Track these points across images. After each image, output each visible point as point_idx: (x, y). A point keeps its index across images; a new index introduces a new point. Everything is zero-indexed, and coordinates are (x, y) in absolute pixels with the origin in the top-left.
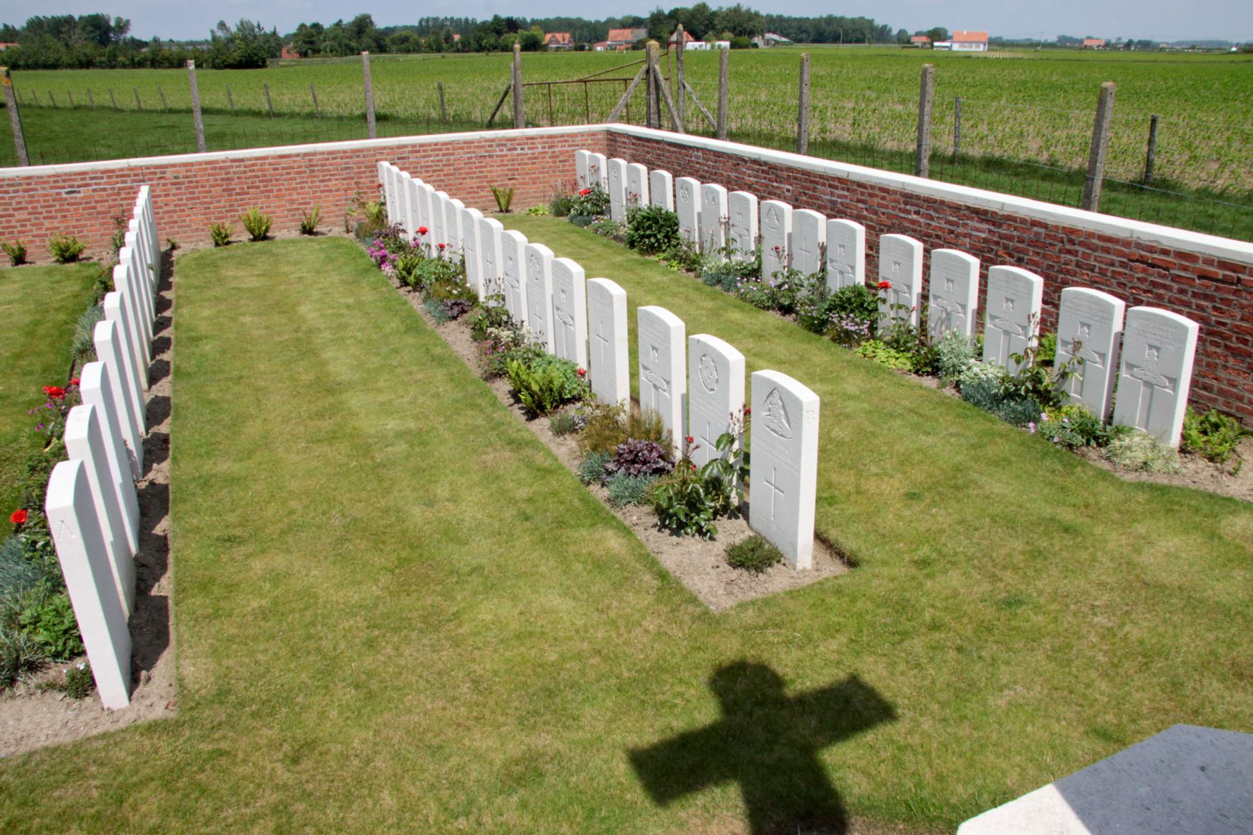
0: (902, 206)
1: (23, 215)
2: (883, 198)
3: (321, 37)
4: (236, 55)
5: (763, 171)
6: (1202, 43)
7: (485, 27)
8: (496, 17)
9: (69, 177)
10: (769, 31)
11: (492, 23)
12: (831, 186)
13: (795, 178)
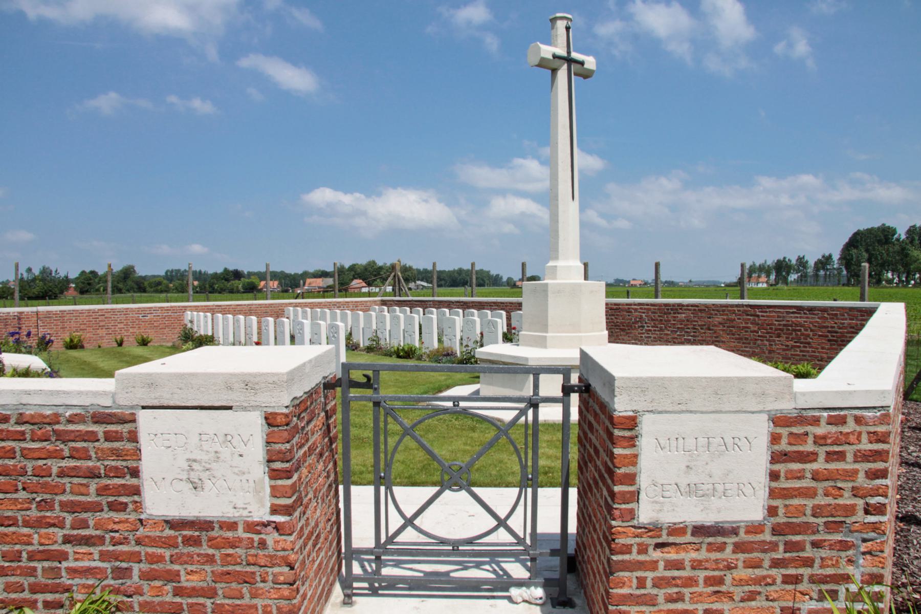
1: (121, 326)
3: (97, 280)
4: (36, 291)
7: (215, 276)
8: (226, 270)
9: (144, 309)
11: (222, 274)
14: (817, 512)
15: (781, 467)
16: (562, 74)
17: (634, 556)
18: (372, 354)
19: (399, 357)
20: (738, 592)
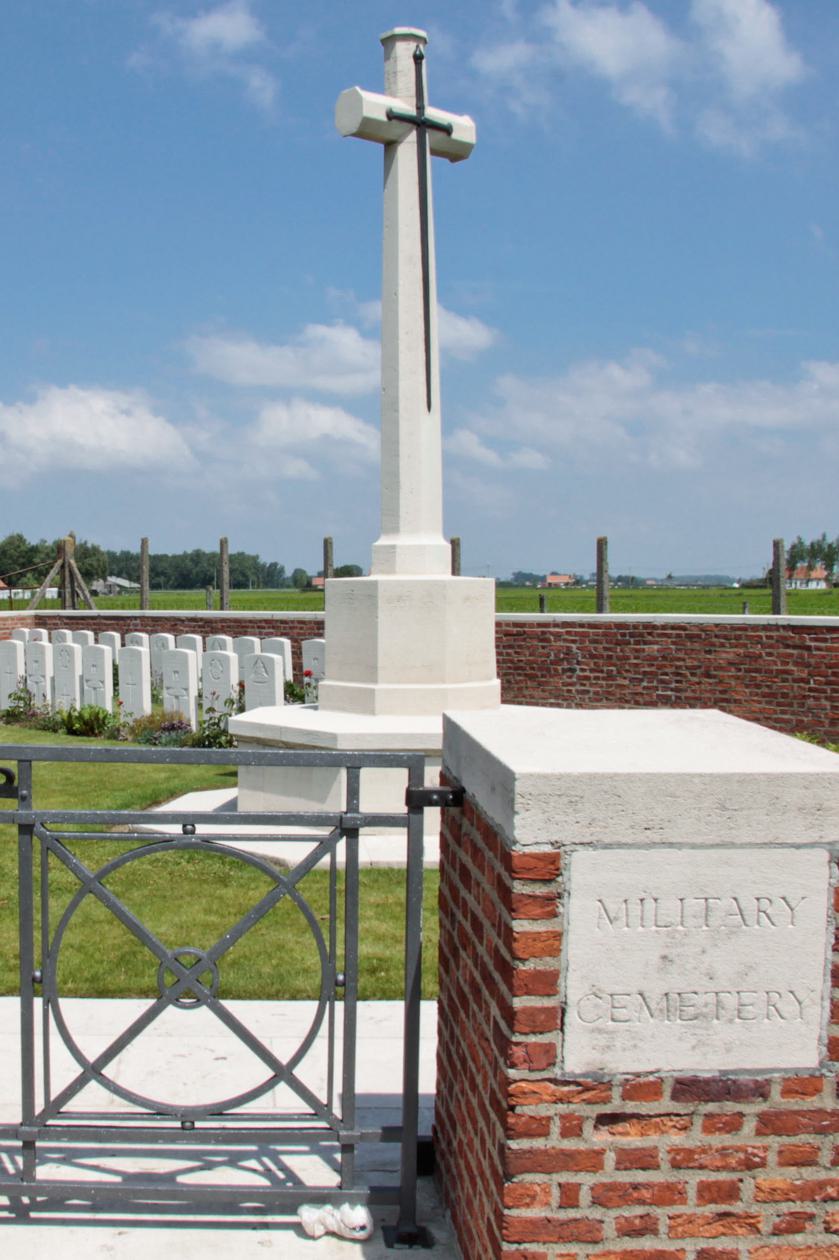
0: (316, 631)
2: (301, 628)
5: (200, 627)
6: (698, 579)
10: (111, 574)
12: (259, 627)
13: (229, 627)
17: (555, 1141)
18: (16, 727)
19: (71, 732)
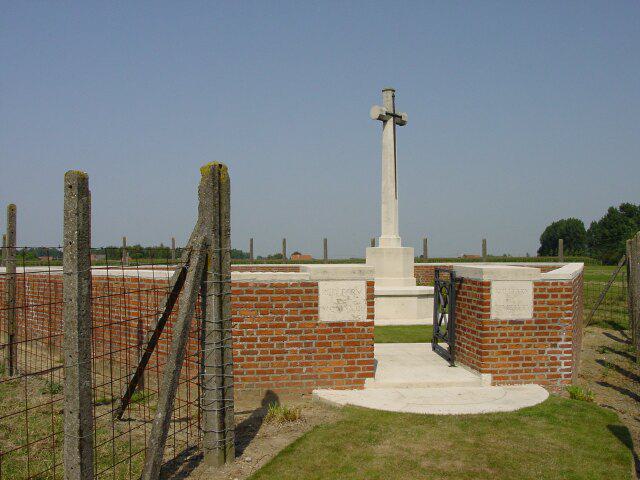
14: (550, 315)
15: (538, 300)
16: (390, 122)
17: (491, 331)
20: (524, 345)
